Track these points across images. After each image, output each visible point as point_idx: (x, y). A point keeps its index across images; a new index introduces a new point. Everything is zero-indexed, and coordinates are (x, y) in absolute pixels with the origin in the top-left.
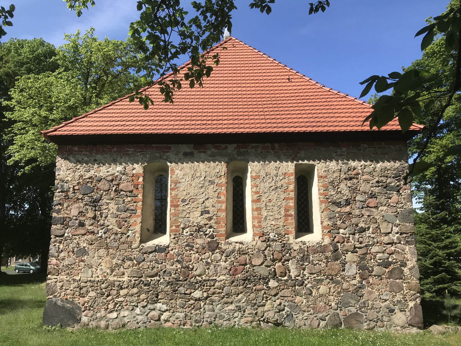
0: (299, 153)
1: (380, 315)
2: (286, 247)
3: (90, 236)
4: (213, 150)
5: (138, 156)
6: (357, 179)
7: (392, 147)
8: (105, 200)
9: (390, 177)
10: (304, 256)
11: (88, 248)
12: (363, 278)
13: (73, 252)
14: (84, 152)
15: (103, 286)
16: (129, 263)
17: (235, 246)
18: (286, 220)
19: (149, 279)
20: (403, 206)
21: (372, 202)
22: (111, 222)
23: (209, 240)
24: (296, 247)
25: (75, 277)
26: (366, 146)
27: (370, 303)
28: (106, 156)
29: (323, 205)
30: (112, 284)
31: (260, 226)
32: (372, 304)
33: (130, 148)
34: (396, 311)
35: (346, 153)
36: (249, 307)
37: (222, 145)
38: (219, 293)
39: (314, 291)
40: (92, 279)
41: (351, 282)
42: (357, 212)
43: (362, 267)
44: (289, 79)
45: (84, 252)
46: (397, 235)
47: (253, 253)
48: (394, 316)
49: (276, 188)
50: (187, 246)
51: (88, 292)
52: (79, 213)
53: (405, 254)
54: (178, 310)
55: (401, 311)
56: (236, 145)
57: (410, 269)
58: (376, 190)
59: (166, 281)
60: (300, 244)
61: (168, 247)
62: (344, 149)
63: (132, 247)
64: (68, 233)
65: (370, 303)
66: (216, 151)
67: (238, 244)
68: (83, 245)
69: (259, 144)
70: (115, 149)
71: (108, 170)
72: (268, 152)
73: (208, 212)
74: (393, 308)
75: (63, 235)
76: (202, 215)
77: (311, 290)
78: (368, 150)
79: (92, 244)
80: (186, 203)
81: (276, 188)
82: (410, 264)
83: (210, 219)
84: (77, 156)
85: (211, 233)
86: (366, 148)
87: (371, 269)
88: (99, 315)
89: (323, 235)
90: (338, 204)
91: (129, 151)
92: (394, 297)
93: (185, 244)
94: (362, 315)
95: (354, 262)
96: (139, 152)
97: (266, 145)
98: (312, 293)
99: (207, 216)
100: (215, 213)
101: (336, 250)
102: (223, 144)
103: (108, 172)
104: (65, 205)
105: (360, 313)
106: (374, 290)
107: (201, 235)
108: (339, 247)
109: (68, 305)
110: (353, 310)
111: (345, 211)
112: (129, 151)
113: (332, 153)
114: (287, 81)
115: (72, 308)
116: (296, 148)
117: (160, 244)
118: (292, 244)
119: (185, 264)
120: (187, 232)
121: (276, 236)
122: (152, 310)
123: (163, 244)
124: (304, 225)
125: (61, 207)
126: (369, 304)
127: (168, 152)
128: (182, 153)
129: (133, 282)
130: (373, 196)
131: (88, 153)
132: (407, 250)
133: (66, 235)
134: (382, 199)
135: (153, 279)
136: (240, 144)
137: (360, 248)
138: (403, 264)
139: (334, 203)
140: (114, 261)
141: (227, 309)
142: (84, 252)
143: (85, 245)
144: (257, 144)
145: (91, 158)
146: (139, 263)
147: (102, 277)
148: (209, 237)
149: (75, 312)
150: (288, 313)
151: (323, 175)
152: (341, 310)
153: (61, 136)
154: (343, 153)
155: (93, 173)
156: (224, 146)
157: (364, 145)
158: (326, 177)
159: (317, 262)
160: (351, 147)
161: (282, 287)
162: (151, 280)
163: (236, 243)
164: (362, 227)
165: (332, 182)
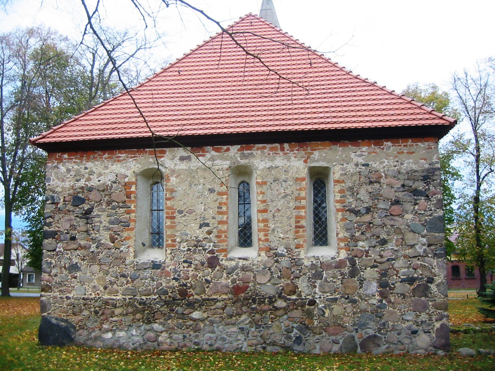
0: (312, 154)
1: (400, 337)
2: (296, 262)
3: (82, 251)
4: (213, 153)
5: (130, 162)
6: (379, 183)
7: (420, 144)
8: (95, 212)
9: (418, 180)
10: (317, 271)
11: (81, 264)
12: (383, 295)
13: (65, 267)
14: (74, 160)
15: (97, 304)
16: (124, 280)
17: (239, 262)
18: (297, 232)
19: (144, 298)
20: (432, 214)
21: (396, 209)
22: (105, 237)
23: (209, 255)
24: (307, 263)
25: (68, 295)
26: (389, 144)
27: (391, 324)
28: (97, 163)
29: (340, 213)
30: (106, 303)
31: (267, 240)
32: (392, 325)
33: (121, 154)
34: (419, 332)
35: (366, 154)
36: (253, 329)
37: (223, 147)
38: (220, 314)
39: (327, 312)
40: (86, 297)
41: (370, 302)
42: (378, 221)
43: (383, 285)
44: (311, 64)
45: (74, 268)
46: (424, 247)
47: (258, 270)
48: (417, 338)
49: (286, 196)
50: (185, 262)
51: (81, 311)
52: (71, 226)
53: (432, 268)
54: (176, 331)
55: (425, 332)
56: (239, 146)
57: (438, 286)
58: (400, 195)
59: (163, 299)
60: (312, 260)
61: (164, 263)
62: (364, 149)
63: (126, 263)
64: (60, 247)
65: (391, 324)
66: (216, 154)
67: (241, 260)
68: (75, 260)
69: (265, 145)
70: (106, 155)
71: (99, 179)
72: (276, 154)
73: (207, 225)
74: (417, 329)
75: (55, 250)
76: (200, 228)
77: (323, 311)
78: (392, 148)
79: (84, 260)
80: (183, 215)
81: (286, 196)
82: (438, 280)
83: (209, 233)
84: (67, 164)
85: (211, 248)
86: (390, 146)
87: (392, 286)
88: (93, 334)
89: (338, 249)
90: (357, 213)
91: (120, 157)
92: (417, 316)
93: (182, 260)
94: (381, 338)
95: (374, 279)
96: (131, 158)
97: (274, 145)
98: (324, 313)
99: (207, 229)
100: (216, 225)
101: (353, 264)
102: (224, 145)
103: (99, 181)
104: (56, 219)
105: (379, 335)
106: (396, 310)
107: (200, 250)
108: (357, 262)
109: (63, 323)
110: (371, 332)
111: (364, 221)
112: (120, 157)
113: (351, 153)
114: (309, 66)
115: (67, 327)
116: (309, 148)
117: (156, 260)
118: (303, 259)
119: (183, 281)
120: (184, 246)
121: (285, 250)
122: (148, 330)
123: (158, 260)
124: (321, 237)
125: (52, 220)
126: (389, 325)
127: (163, 157)
128: (178, 157)
129: (128, 300)
130: (397, 202)
131: (78, 161)
132: (435, 264)
133: (58, 250)
134: (409, 207)
135: (148, 297)
136: (244, 146)
137: (381, 263)
138: (430, 280)
139: (352, 211)
140: (108, 278)
141: (229, 330)
142: (74, 268)
143: (77, 261)
144: (263, 145)
145: (81, 166)
146: (133, 280)
147: (95, 295)
148: (209, 252)
149: (70, 331)
150: (297, 335)
151: (341, 180)
152: (357, 332)
153: (50, 143)
154: (364, 153)
155: (84, 183)
156: (225, 147)
157: (387, 143)
158: (343, 182)
159: (331, 279)
160: (372, 146)
161: (291, 307)
162: (147, 299)
163: (240, 259)
164: (384, 238)
165: (351, 189)
